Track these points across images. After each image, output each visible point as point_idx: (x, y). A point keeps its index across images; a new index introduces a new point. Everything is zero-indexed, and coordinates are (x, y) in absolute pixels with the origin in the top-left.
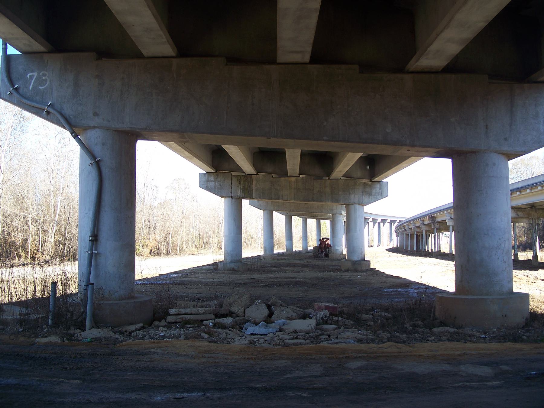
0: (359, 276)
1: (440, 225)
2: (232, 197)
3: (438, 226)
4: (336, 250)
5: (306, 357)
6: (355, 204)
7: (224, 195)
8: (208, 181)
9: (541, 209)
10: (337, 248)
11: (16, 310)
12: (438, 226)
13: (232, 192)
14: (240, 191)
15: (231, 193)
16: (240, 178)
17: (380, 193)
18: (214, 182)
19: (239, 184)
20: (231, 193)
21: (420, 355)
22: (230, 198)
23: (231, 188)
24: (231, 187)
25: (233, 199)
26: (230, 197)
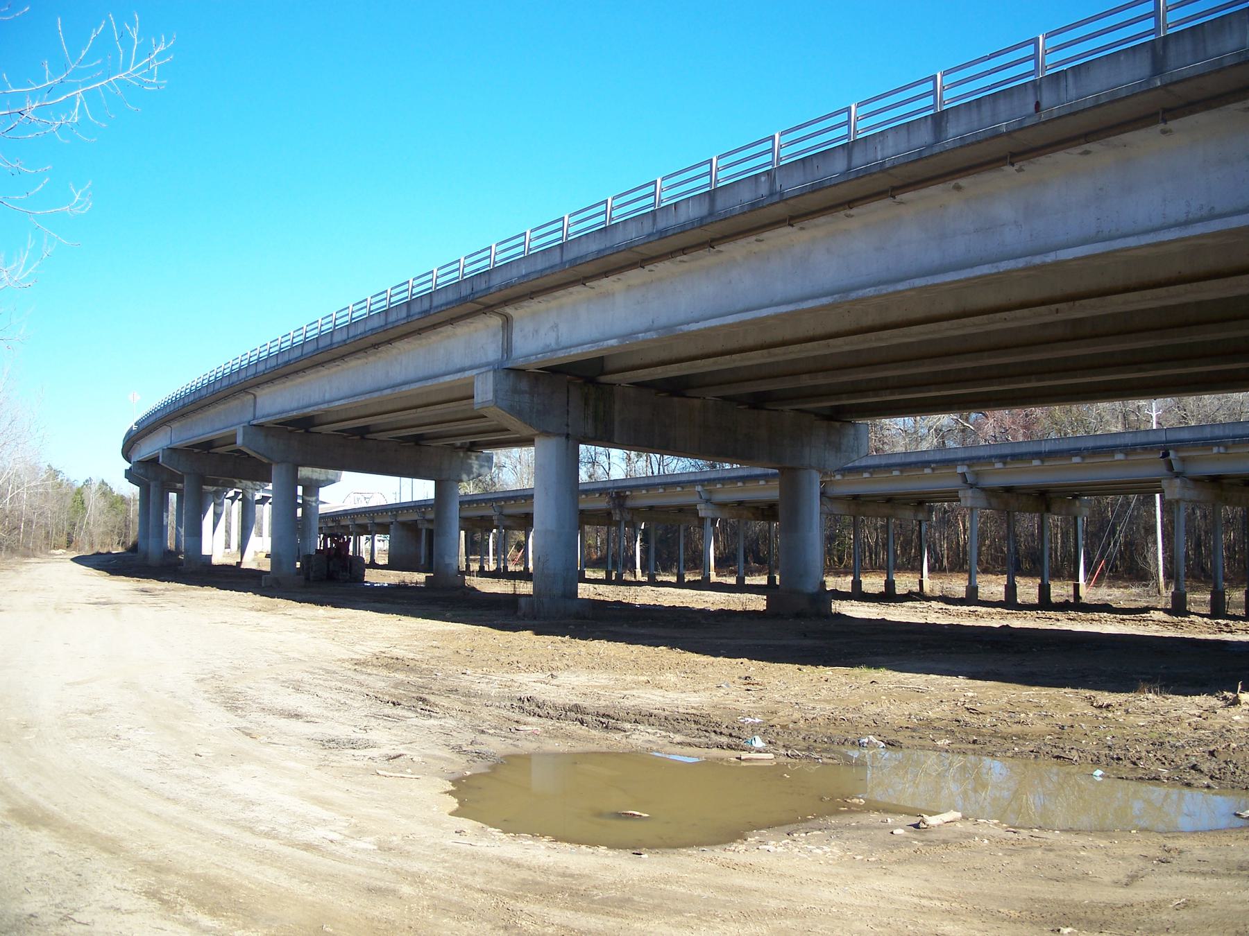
0: (571, 627)
1: (633, 514)
2: (567, 436)
3: (628, 517)
4: (448, 565)
5: (1069, 896)
6: (812, 467)
7: (550, 430)
8: (515, 391)
9: (1024, 494)
10: (447, 560)
11: (374, 933)
12: (628, 517)
13: (570, 424)
14: (587, 422)
15: (568, 425)
16: (586, 391)
17: (855, 448)
18: (528, 395)
19: (585, 404)
20: (568, 425)
21: (424, 823)
22: (564, 438)
23: (568, 414)
24: (568, 411)
25: (570, 441)
26: (563, 434)
